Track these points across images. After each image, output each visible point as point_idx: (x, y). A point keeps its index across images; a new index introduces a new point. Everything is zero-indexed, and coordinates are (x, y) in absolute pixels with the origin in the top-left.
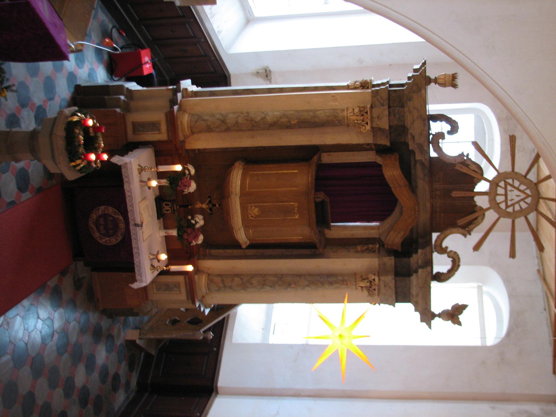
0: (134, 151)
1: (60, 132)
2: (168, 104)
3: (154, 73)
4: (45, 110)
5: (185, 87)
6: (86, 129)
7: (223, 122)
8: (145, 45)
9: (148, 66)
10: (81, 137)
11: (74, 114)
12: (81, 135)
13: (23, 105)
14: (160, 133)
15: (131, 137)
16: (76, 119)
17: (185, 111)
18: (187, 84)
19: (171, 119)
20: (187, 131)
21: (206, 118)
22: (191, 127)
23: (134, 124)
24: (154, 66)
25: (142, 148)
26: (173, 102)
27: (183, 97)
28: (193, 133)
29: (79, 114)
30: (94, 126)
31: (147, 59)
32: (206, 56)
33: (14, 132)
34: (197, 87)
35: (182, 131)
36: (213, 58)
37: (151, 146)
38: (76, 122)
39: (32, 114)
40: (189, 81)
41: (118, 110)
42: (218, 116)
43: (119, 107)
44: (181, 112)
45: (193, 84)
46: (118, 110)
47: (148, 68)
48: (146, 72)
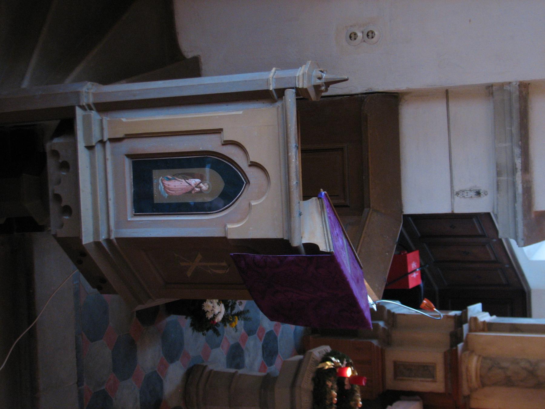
0: (395, 404)
1: (306, 383)
2: (446, 339)
3: (422, 285)
4: (276, 338)
5: (474, 316)
6: (341, 380)
7: (532, 373)
8: (411, 245)
9: (415, 275)
10: (335, 393)
11: (326, 358)
12: (334, 389)
13: (250, 332)
14: (435, 381)
15: (391, 384)
16: (329, 365)
17: (472, 352)
18: (476, 310)
19: (453, 364)
20: (475, 382)
21: (505, 364)
22: (481, 376)
23: (397, 365)
24: (423, 275)
25: (405, 400)
26: (456, 337)
27: (470, 330)
28: (483, 385)
29: (333, 359)
30: (353, 377)
31: (414, 265)
32: (496, 262)
33: (241, 375)
34: (491, 315)
35: (468, 381)
36: (507, 266)
37: (418, 397)
38: (330, 369)
39: (260, 344)
40: (478, 306)
41: (375, 342)
42: (523, 364)
43: (375, 337)
44: (467, 353)
45: (484, 309)
46: (375, 342)
47: (414, 279)
48: (412, 284)
